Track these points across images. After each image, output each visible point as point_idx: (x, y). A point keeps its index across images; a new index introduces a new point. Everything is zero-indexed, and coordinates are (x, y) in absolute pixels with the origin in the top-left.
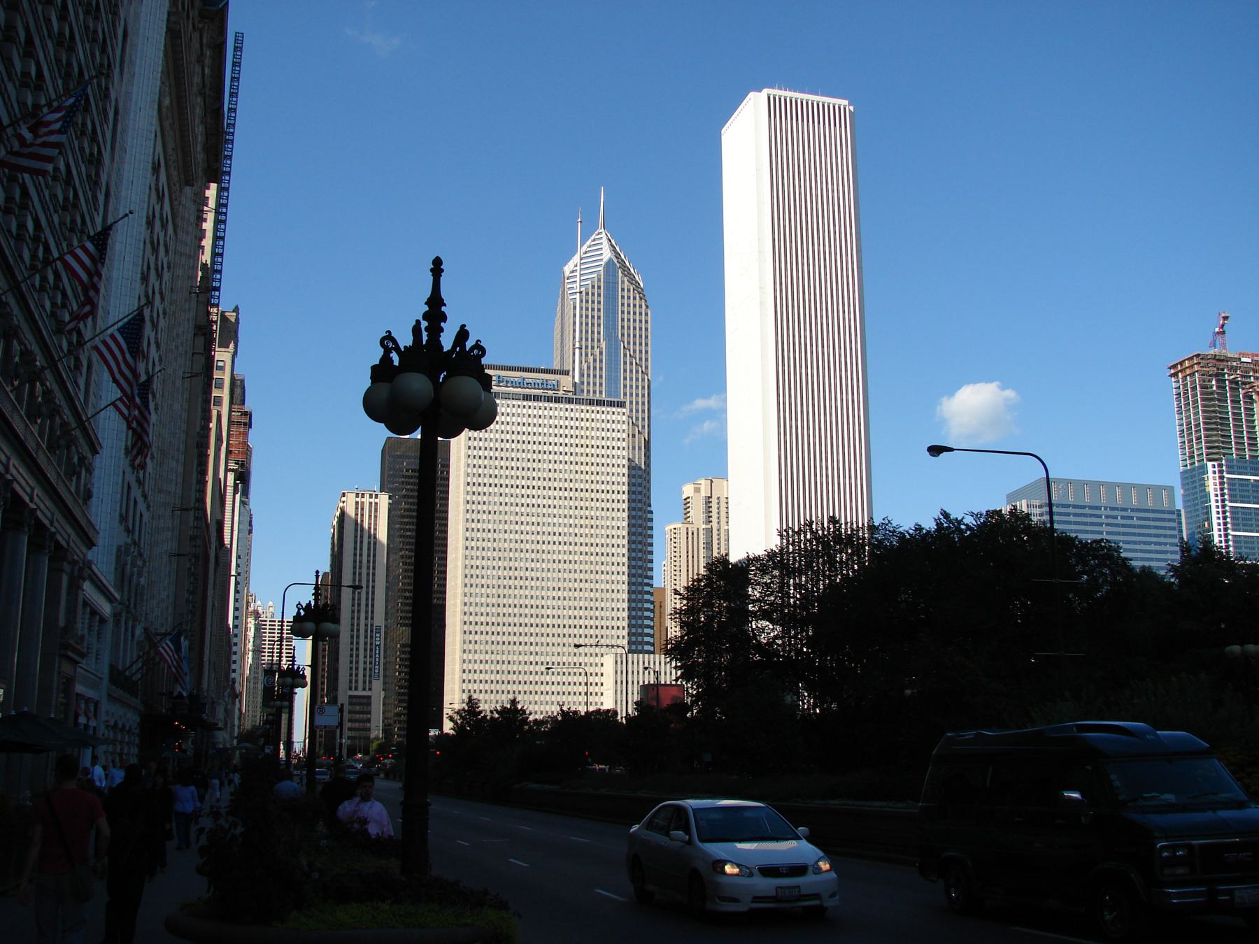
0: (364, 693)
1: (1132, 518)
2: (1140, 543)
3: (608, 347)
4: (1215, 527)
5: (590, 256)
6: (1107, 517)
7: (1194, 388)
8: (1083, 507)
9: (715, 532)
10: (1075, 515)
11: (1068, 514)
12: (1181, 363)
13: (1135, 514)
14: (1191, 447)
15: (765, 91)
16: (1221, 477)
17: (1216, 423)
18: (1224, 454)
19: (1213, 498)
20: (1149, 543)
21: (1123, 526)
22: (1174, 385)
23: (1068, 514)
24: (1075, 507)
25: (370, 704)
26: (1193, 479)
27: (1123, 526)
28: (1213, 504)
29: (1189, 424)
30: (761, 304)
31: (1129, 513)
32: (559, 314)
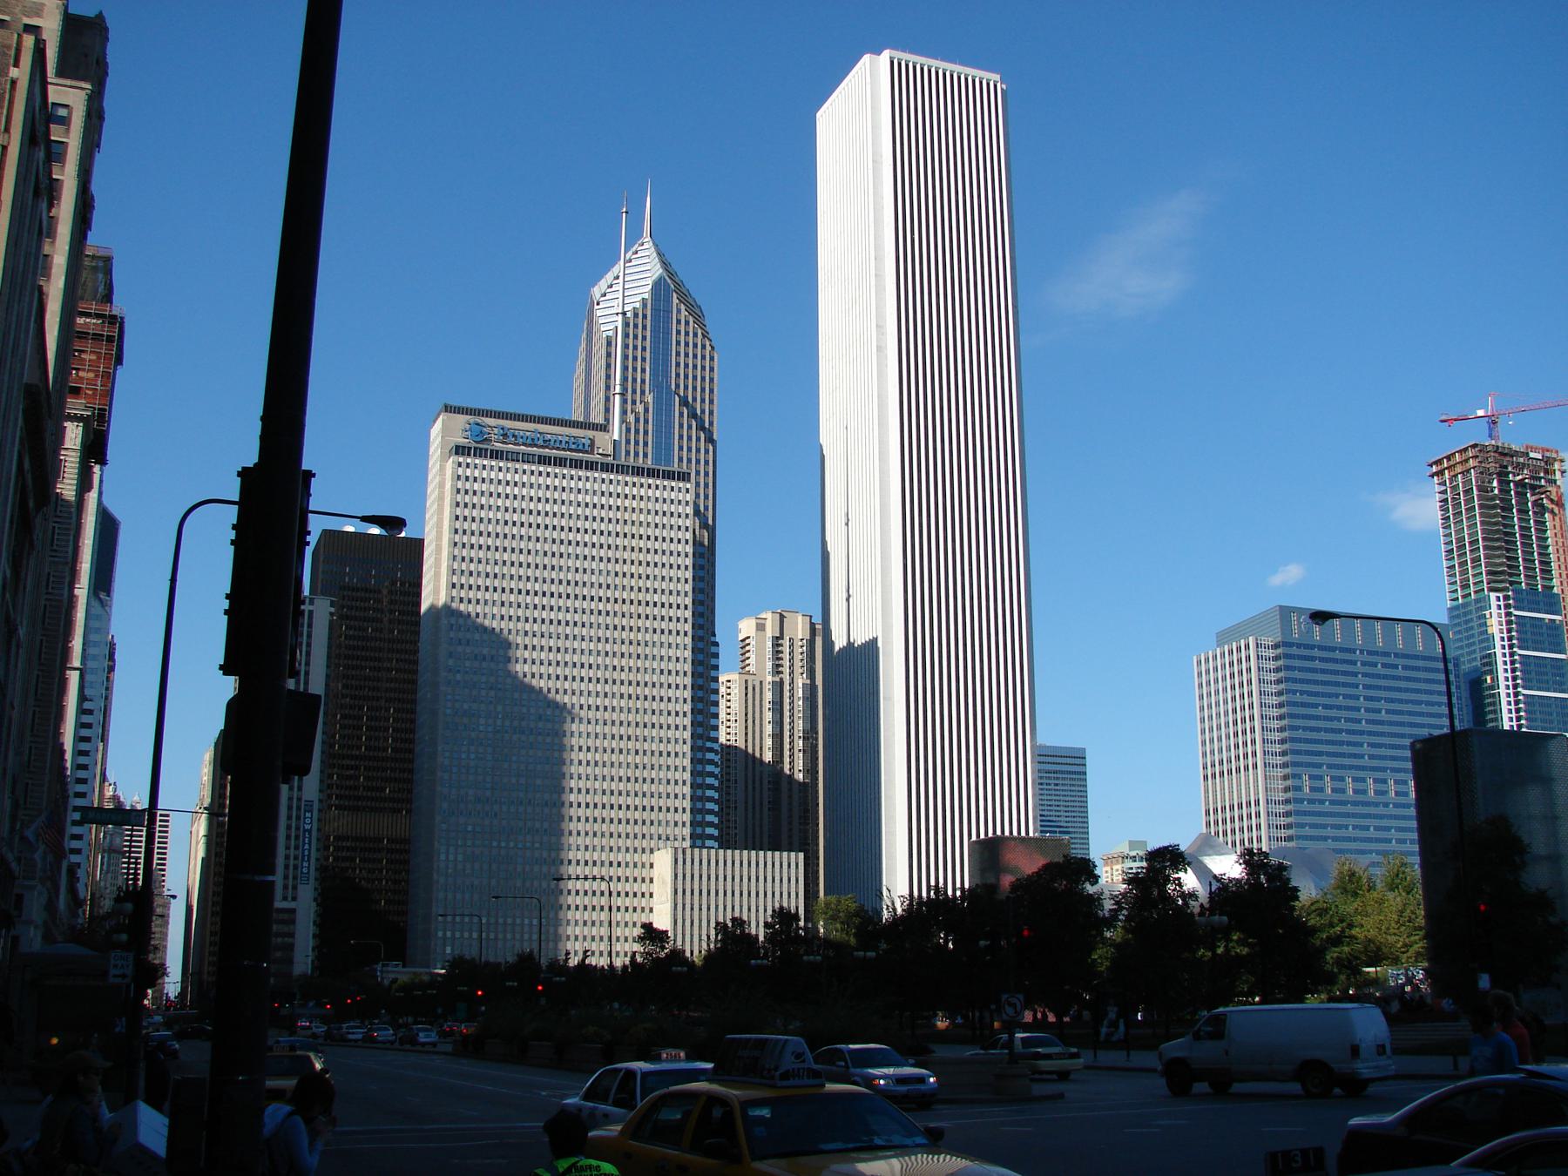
0: (285, 905)
1: (1396, 667)
2: (1407, 702)
3: (657, 401)
4: (1502, 683)
5: (629, 282)
6: (1364, 664)
7: (1468, 492)
8: (1333, 649)
9: (787, 687)
10: (1322, 660)
11: (1313, 659)
12: (1448, 458)
13: (1400, 661)
14: (1464, 572)
15: (886, 55)
16: (1508, 614)
17: (1500, 538)
18: (1511, 583)
19: (1498, 643)
20: (1420, 703)
21: (1385, 677)
22: (1438, 488)
23: (1313, 659)
24: (1322, 648)
25: (293, 922)
26: (1468, 615)
27: (1385, 677)
28: (1498, 651)
29: (1460, 540)
30: (880, 349)
31: (1391, 660)
32: (582, 357)
